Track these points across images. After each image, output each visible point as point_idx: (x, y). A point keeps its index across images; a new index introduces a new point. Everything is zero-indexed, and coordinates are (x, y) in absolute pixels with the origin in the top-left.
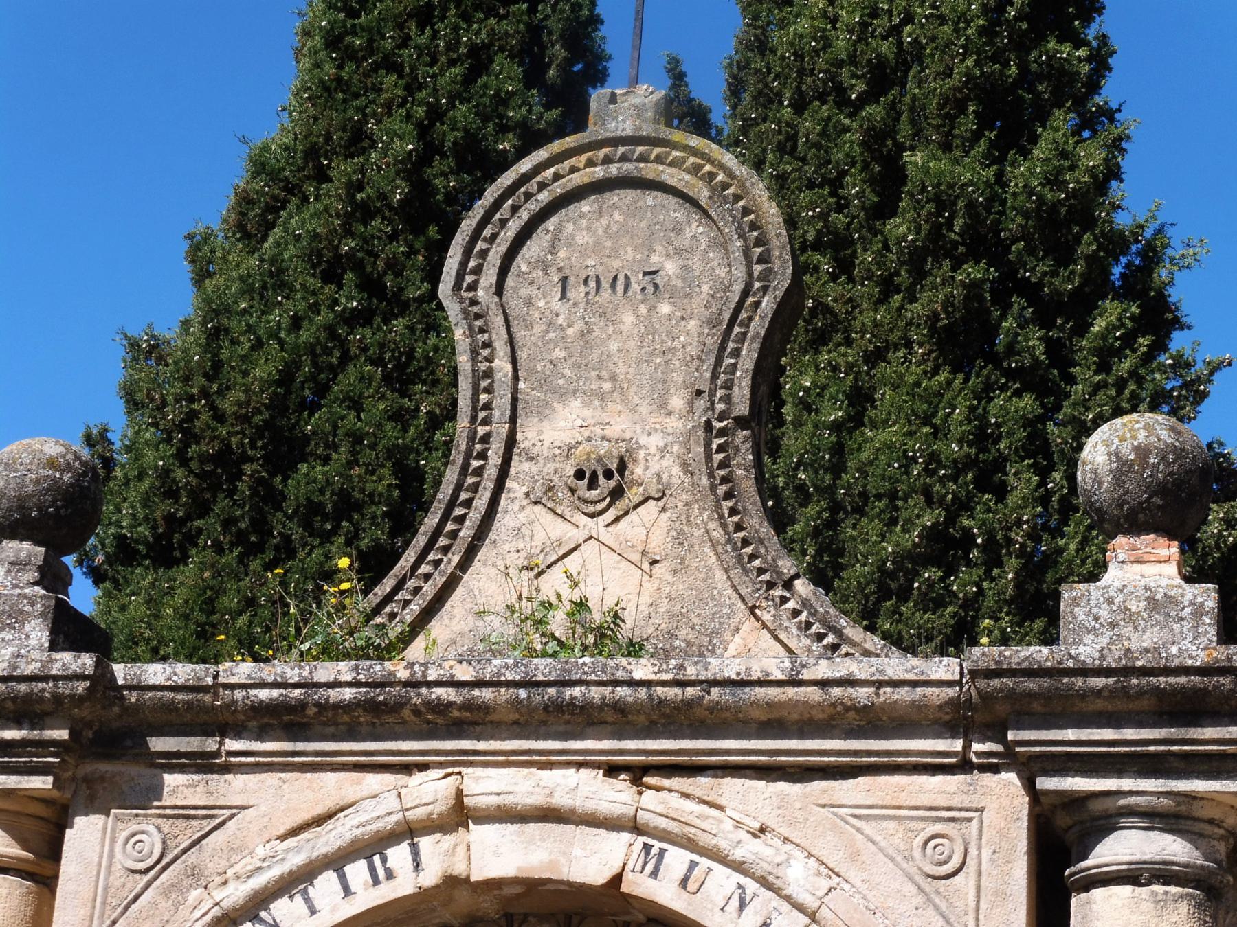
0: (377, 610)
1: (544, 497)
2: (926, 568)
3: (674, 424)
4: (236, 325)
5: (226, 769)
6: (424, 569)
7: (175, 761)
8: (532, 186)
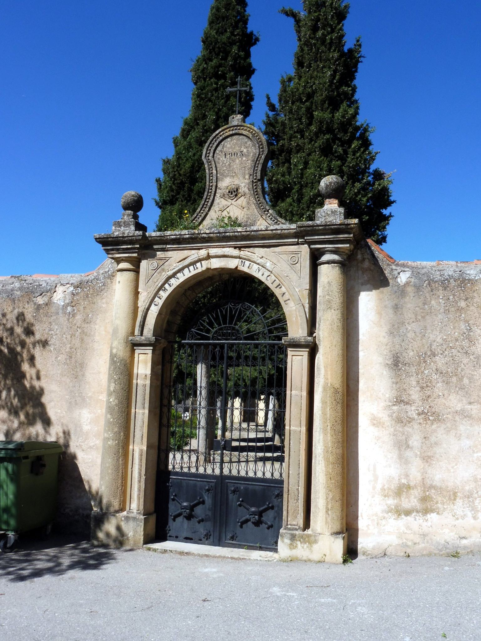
0: (194, 220)
1: (223, 196)
2: (319, 197)
3: (247, 181)
4: (183, 156)
5: (167, 251)
6: (202, 211)
7: (158, 250)
8: (219, 136)
